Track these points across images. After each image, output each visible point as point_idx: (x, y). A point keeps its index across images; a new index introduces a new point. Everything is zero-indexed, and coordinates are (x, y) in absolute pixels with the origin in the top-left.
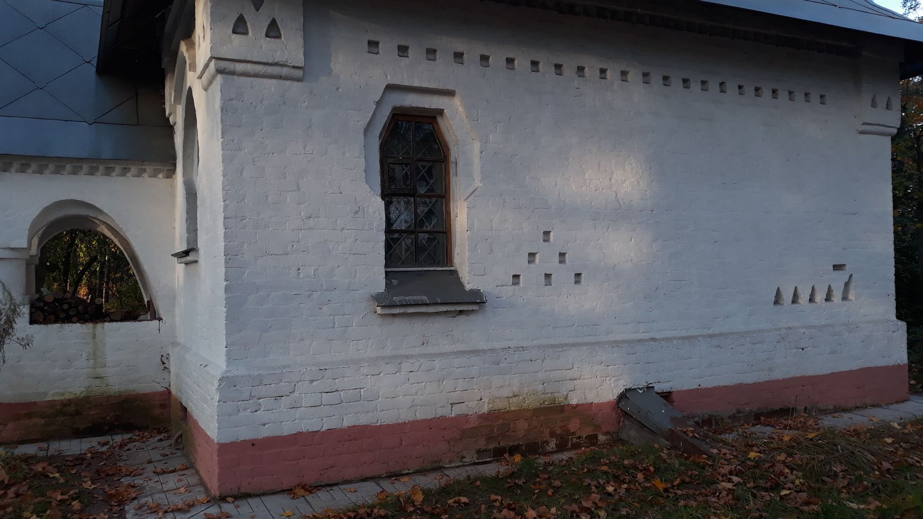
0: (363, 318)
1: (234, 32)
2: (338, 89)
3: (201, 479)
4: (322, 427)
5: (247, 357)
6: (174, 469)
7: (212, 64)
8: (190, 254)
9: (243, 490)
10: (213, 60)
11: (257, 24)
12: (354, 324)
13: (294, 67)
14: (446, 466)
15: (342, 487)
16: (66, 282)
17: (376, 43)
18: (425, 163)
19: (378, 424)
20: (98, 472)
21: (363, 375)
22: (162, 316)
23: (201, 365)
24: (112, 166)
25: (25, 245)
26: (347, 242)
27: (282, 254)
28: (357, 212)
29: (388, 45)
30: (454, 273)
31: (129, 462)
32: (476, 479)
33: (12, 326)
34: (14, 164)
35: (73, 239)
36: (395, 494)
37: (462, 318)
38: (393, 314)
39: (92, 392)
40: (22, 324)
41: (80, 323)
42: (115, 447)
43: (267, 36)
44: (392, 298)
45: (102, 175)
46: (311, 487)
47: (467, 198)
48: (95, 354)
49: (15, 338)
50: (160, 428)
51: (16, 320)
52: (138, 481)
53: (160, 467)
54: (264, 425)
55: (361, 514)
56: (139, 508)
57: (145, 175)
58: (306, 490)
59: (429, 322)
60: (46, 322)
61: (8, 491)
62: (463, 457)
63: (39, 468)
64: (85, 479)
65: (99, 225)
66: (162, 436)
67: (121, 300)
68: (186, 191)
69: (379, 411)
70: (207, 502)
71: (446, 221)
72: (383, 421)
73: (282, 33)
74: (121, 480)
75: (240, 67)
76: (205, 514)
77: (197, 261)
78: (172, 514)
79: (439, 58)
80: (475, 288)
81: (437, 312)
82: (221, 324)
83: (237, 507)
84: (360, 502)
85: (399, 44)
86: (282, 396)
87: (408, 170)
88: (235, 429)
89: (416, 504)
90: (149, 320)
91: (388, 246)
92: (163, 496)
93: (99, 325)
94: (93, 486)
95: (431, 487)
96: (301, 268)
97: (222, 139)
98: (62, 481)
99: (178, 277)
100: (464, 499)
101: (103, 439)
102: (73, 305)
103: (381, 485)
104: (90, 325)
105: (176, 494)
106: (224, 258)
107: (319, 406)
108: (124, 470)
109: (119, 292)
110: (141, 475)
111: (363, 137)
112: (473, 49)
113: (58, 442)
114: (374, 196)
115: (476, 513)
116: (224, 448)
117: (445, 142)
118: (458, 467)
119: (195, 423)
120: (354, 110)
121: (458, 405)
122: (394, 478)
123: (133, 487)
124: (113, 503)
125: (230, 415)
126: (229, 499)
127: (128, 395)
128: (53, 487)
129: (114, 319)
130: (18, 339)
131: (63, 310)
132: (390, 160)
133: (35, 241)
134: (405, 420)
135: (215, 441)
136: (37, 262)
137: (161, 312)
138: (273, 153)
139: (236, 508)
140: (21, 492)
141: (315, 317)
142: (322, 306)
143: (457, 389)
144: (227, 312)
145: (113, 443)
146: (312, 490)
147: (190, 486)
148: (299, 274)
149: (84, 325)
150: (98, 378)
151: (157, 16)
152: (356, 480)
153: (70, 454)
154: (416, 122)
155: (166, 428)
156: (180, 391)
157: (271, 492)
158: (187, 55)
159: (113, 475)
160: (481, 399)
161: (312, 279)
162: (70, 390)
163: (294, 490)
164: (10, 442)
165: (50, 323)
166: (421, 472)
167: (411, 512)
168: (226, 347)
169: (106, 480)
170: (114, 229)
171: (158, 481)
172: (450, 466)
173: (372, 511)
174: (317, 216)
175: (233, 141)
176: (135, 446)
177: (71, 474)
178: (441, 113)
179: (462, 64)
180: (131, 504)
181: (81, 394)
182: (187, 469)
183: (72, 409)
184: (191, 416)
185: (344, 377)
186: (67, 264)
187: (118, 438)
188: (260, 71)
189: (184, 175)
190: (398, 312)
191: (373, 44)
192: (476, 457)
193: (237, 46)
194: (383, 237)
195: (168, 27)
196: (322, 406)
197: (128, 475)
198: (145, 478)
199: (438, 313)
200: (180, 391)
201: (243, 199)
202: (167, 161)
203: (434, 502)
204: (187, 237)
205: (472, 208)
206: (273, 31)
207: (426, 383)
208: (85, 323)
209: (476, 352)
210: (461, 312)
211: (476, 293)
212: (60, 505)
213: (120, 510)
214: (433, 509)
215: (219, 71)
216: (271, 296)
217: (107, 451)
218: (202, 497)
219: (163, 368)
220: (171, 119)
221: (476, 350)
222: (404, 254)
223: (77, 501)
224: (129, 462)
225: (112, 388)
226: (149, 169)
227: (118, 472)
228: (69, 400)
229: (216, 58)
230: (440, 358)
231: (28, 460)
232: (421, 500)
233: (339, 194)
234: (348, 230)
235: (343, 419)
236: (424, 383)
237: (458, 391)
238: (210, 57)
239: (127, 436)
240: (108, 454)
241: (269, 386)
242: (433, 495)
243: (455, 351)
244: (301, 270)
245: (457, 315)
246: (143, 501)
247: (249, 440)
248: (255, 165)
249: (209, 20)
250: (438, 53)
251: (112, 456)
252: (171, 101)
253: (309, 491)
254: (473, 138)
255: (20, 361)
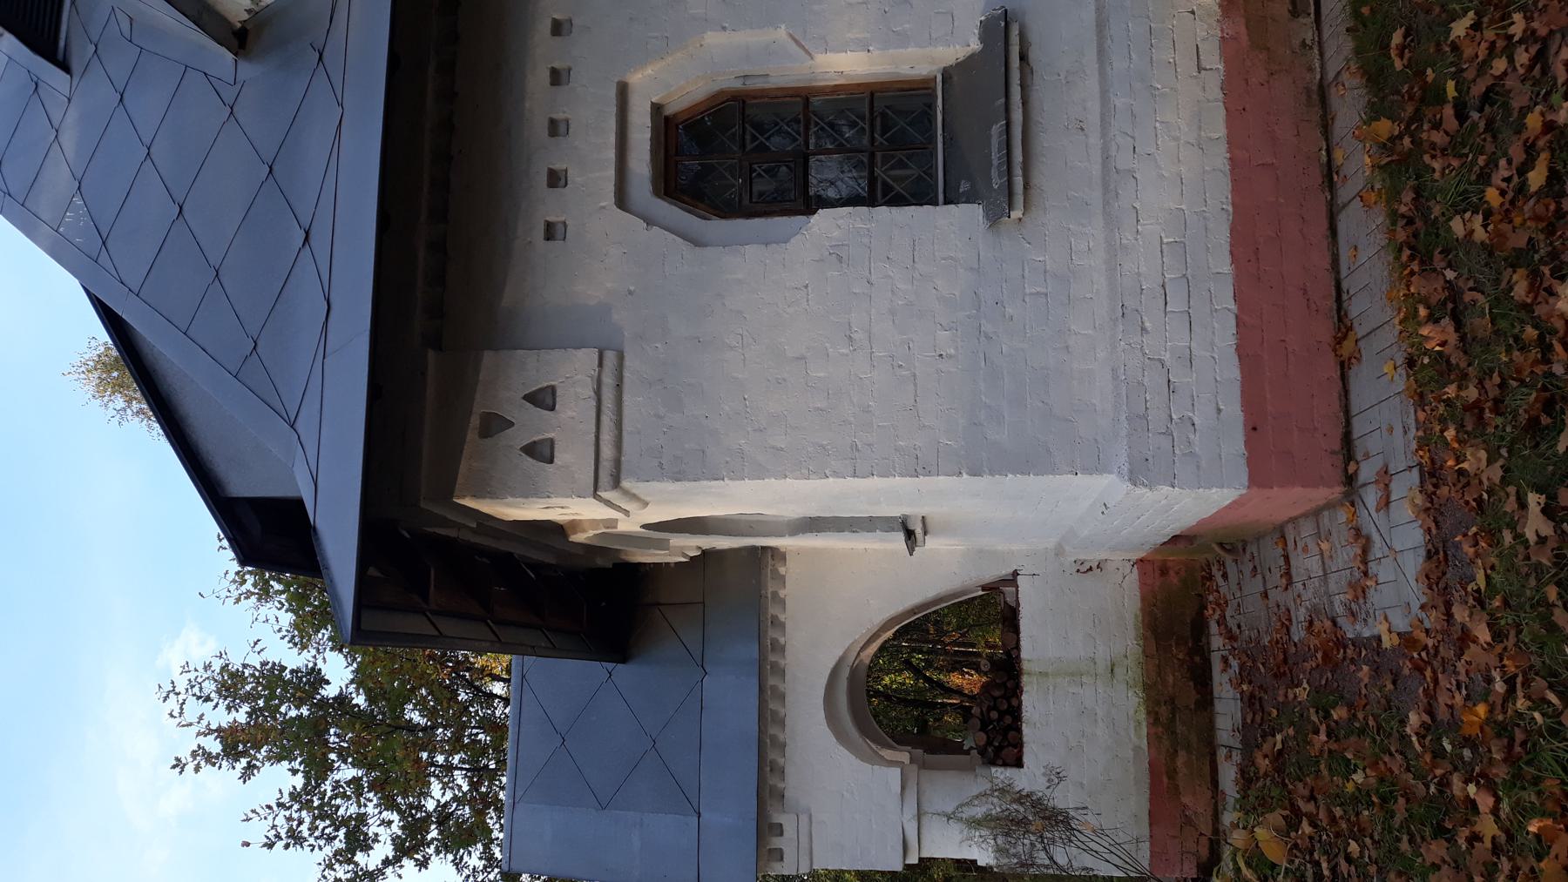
0: (1029, 243)
1: (551, 461)
2: (630, 293)
3: (1305, 515)
4: (1229, 310)
5: (1096, 440)
6: (1282, 558)
7: (604, 495)
8: (911, 528)
9: (1337, 446)
10: (599, 493)
11: (530, 424)
12: (1041, 259)
13: (601, 364)
14: (1318, 77)
15: (1344, 272)
16: (944, 705)
17: (548, 225)
18: (748, 137)
19: (1230, 209)
20: (1278, 676)
21: (1137, 240)
22: (1011, 570)
23: (1103, 513)
24: (769, 641)
25: (895, 772)
26: (892, 274)
27: (915, 385)
28: (840, 259)
29: (550, 207)
30: (947, 74)
31: (1262, 627)
32: (1356, 14)
33: (1028, 796)
34: (771, 783)
35: (877, 694)
36: (1367, 174)
37: (1034, 55)
38: (1025, 188)
39: (1137, 679)
40: (1027, 778)
41: (1021, 695)
42: (1233, 647)
43: (552, 408)
44: (995, 190)
45: (784, 657)
46: (1339, 329)
47: (807, 52)
48: (1072, 674)
49: (1048, 792)
50: (1203, 577)
51: (1017, 789)
52: (1301, 614)
53: (1276, 578)
54: (1219, 411)
55: (1408, 237)
56: (1353, 616)
57: (782, 593)
58: (1345, 337)
59: (1041, 120)
60: (1019, 745)
61: (1304, 811)
62: (1304, 44)
63: (1264, 764)
64: (1291, 696)
65: (861, 661)
66: (1218, 575)
67: (972, 626)
68: (806, 532)
69: (1205, 209)
70: (1353, 504)
71: (852, 94)
72: (1224, 200)
73: (545, 384)
74: (1296, 641)
75: (607, 452)
76: (1378, 511)
77: (923, 517)
78: (1371, 564)
79: (564, 112)
80: (976, 31)
81: (1023, 103)
82: (1033, 482)
83: (1367, 456)
84: (1381, 239)
85: (546, 186)
86: (1169, 381)
87: (760, 167)
88: (1223, 460)
89: (1396, 133)
90: (1017, 591)
91: (897, 201)
92: (1333, 578)
93: (1025, 666)
94: (1305, 685)
95: (1363, 102)
96: (938, 353)
97: (726, 479)
98: (1291, 731)
99: (946, 545)
100: (1397, 38)
101: (1217, 666)
102: (992, 704)
103: (1346, 201)
104: (1025, 679)
105: (1331, 557)
106: (922, 477)
107: (1190, 317)
108: (1278, 636)
109: (959, 628)
110: (1289, 611)
111: (709, 248)
112: (543, 52)
113: (1217, 731)
114: (811, 228)
115: (1428, 12)
116: (1259, 477)
117: (708, 99)
118: (1321, 54)
119: (1202, 523)
120: (663, 264)
121: (1201, 58)
122: (1335, 177)
123: (1311, 623)
124: (1340, 656)
125: (1198, 467)
126: (1351, 469)
127: (1143, 625)
128: (1301, 744)
129: (1014, 642)
130: (1048, 788)
131: (1000, 719)
132: (746, 201)
133: (888, 754)
134: (1225, 158)
135: (1244, 492)
136: (919, 752)
137: (1004, 572)
138: (745, 399)
139: (1369, 458)
140: (1306, 793)
141: (1027, 327)
142: (1007, 317)
143: (1171, 60)
144: (1014, 473)
145: (1226, 650)
146: (1346, 327)
147: (1319, 533)
148: (950, 357)
149: (1025, 689)
150: (1112, 670)
151: (533, 576)
152: (1334, 246)
153: (1240, 715)
154: (677, 155)
155: (1202, 567)
156: (1143, 544)
157: (1343, 398)
158: (591, 531)
159: (1285, 652)
160: (1193, 12)
161: (959, 333)
162: (1131, 712)
163: (1342, 359)
164: (1213, 801)
165: (1021, 739)
166: (1326, 128)
167: (1412, 142)
168: (1076, 474)
169: (1294, 664)
170: (870, 638)
171: (1304, 585)
172: (1319, 70)
173: (1403, 216)
174: (848, 327)
175: (727, 462)
176: (1232, 617)
177: (1277, 716)
178: (659, 108)
179: (569, 70)
180: (1343, 629)
181: (1139, 697)
182: (1283, 537)
183: (1164, 711)
184: (1190, 529)
185: (1139, 274)
186: (915, 703)
187: (1217, 642)
188: (611, 419)
189: (781, 535)
190: (1021, 178)
191: (550, 232)
192: (1304, 18)
193: (573, 456)
194: (883, 212)
195: (550, 559)
196: (1190, 311)
197: (1288, 630)
198: (1295, 603)
199: (1025, 103)
200: (1143, 544)
201: (823, 447)
202: (759, 562)
203: (1396, 98)
204: (749, 479)
205: (826, 41)
206: (543, 399)
207: (1156, 121)
208: (1022, 687)
209: (1101, 26)
210: (1023, 57)
211: (987, 30)
212: (1336, 736)
213: (1353, 645)
214: (1411, 98)
215: (616, 483)
216: (987, 401)
217: (1239, 659)
218: (1342, 515)
219: (1099, 570)
220: (692, 554)
221: (1097, 26)
222: (908, 172)
223: (1332, 712)
224: (1262, 627)
225: (1131, 650)
226: (771, 587)
227: (1280, 646)
228: (1149, 713)
229: (596, 488)
230: (1111, 95)
231: (1247, 778)
232: (1389, 123)
233: (809, 288)
234: (870, 273)
235: (1218, 273)
236: (1158, 125)
237: (1174, 58)
238: (594, 498)
239: (1214, 628)
240: (1245, 658)
241: (1148, 404)
242: (1383, 99)
243: (1097, 66)
244: (942, 353)
245: (1029, 65)
246: (1340, 610)
247: (1246, 435)
248: (765, 428)
249: (535, 499)
250: (555, 116)
251: (1249, 652)
252: (664, 555)
253: (1347, 331)
254: (698, 45)
255: (1081, 784)
